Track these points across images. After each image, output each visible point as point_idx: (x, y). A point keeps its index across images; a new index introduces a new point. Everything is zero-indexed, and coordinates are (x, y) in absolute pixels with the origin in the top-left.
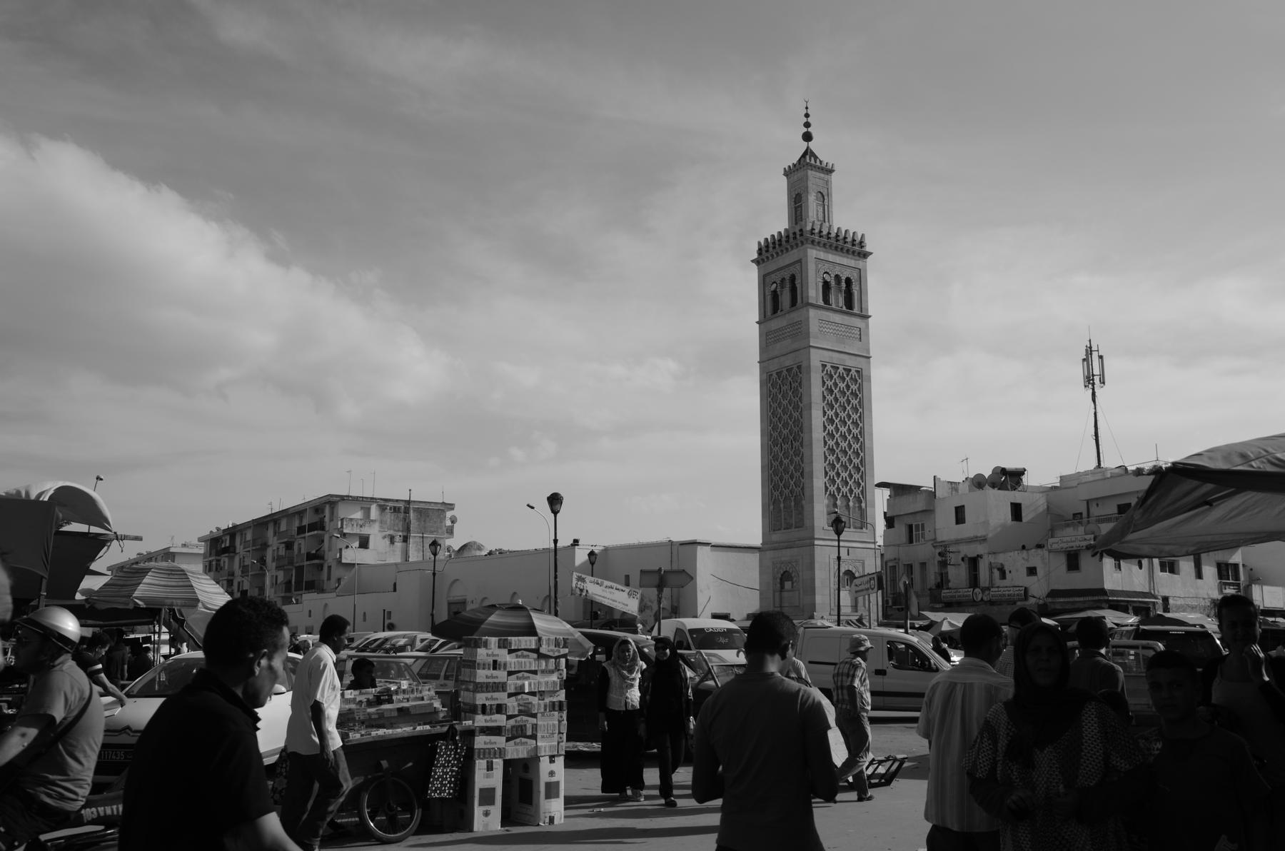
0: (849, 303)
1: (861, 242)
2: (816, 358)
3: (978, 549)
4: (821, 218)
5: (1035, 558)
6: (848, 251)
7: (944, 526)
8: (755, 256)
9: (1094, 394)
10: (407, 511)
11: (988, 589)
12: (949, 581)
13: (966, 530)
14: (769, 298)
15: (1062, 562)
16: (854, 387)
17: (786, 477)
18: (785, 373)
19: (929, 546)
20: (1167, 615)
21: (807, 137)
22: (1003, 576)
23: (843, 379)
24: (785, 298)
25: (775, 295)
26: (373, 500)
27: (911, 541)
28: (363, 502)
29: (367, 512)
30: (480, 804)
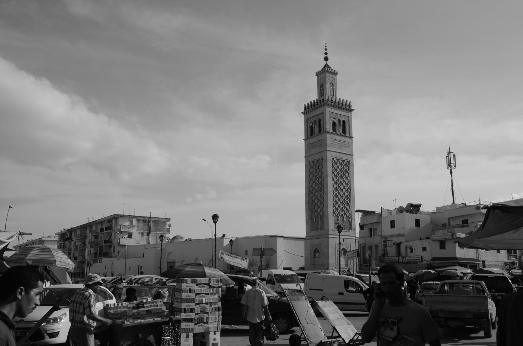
0: (344, 131)
1: (349, 105)
2: (330, 155)
3: (401, 239)
7: (386, 229)
8: (303, 111)
9: (451, 171)
10: (149, 222)
12: (388, 253)
13: (395, 231)
14: (309, 129)
15: (438, 245)
17: (316, 207)
18: (316, 162)
19: (379, 237)
20: (485, 269)
21: (326, 59)
22: (412, 251)
24: (316, 129)
25: (312, 128)
26: (134, 217)
27: (371, 236)
28: (130, 218)
29: (131, 222)
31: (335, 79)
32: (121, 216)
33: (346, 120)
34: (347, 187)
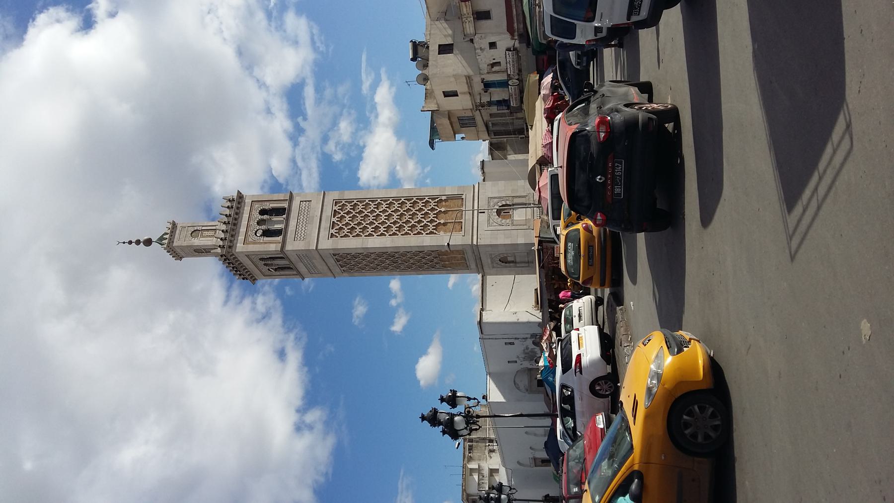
0: (279, 211)
1: (229, 200)
2: (327, 244)
3: (477, 80)
4: (212, 233)
5: (482, 42)
6: (237, 214)
7: (461, 104)
10: (471, 441)
11: (509, 75)
13: (461, 88)
14: (278, 273)
15: (484, 23)
16: (349, 207)
21: (148, 242)
22: (498, 64)
23: (342, 217)
26: (464, 467)
30: (673, 114)
31: (183, 227)
32: (464, 490)
33: (258, 207)
34: (384, 206)
